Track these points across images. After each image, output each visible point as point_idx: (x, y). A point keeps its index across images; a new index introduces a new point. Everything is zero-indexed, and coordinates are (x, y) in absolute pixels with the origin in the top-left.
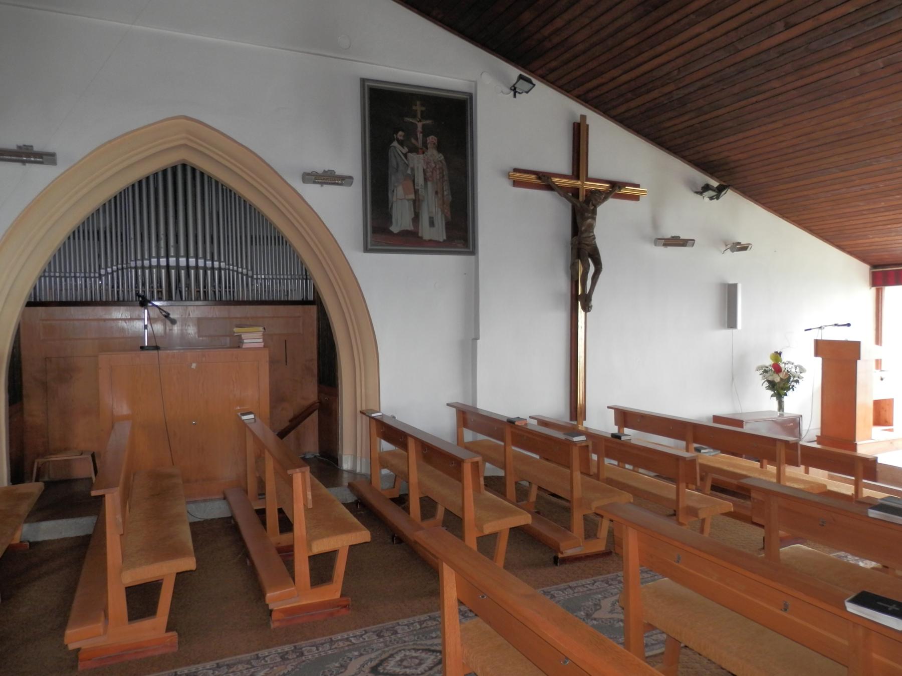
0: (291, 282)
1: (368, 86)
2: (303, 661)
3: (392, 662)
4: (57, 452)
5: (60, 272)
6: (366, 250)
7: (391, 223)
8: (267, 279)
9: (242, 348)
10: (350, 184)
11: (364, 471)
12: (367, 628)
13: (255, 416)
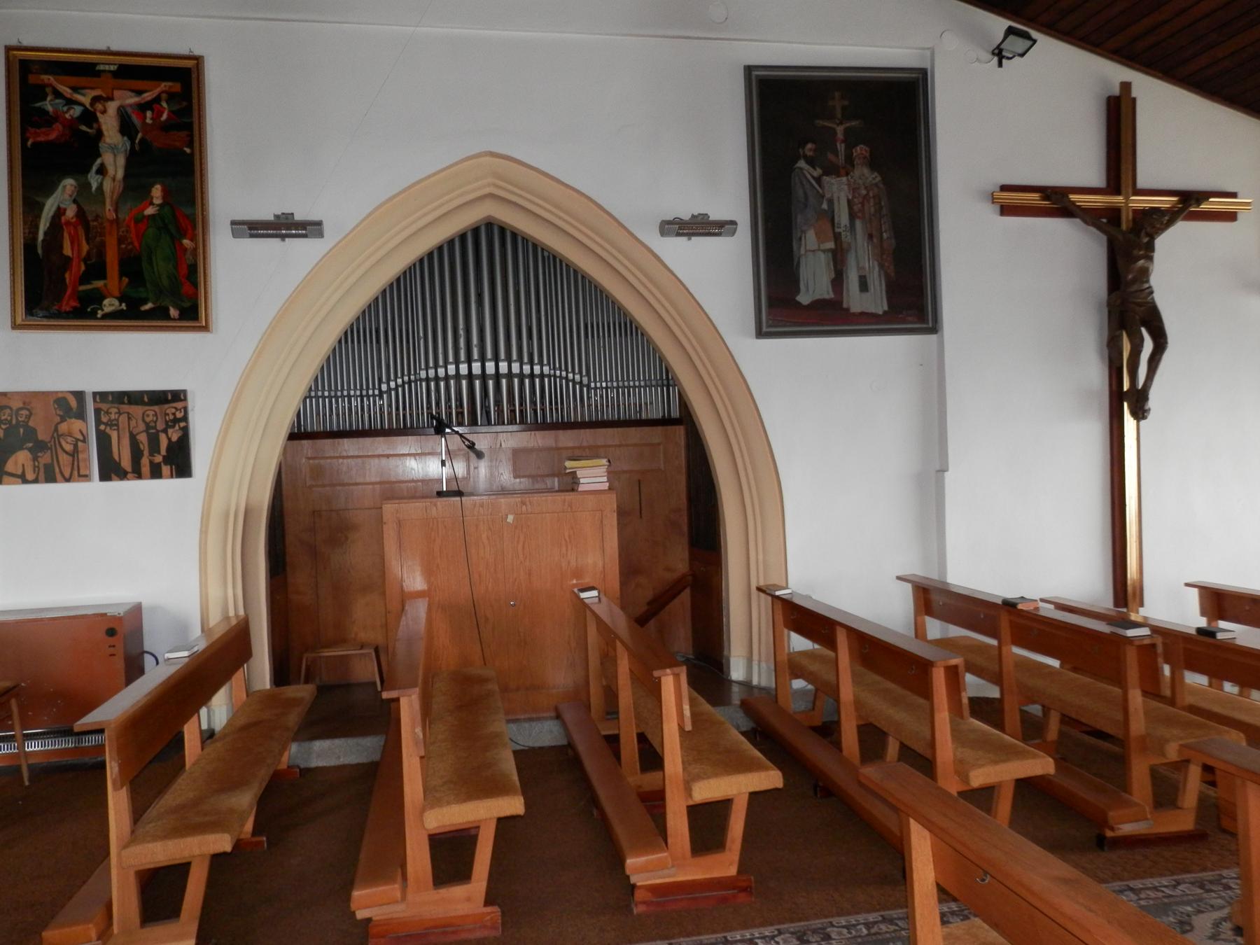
0: (645, 391)
1: (757, 76)
5: (330, 390)
6: (760, 334)
7: (798, 291)
8: (610, 388)
9: (577, 491)
10: (733, 233)
11: (764, 683)
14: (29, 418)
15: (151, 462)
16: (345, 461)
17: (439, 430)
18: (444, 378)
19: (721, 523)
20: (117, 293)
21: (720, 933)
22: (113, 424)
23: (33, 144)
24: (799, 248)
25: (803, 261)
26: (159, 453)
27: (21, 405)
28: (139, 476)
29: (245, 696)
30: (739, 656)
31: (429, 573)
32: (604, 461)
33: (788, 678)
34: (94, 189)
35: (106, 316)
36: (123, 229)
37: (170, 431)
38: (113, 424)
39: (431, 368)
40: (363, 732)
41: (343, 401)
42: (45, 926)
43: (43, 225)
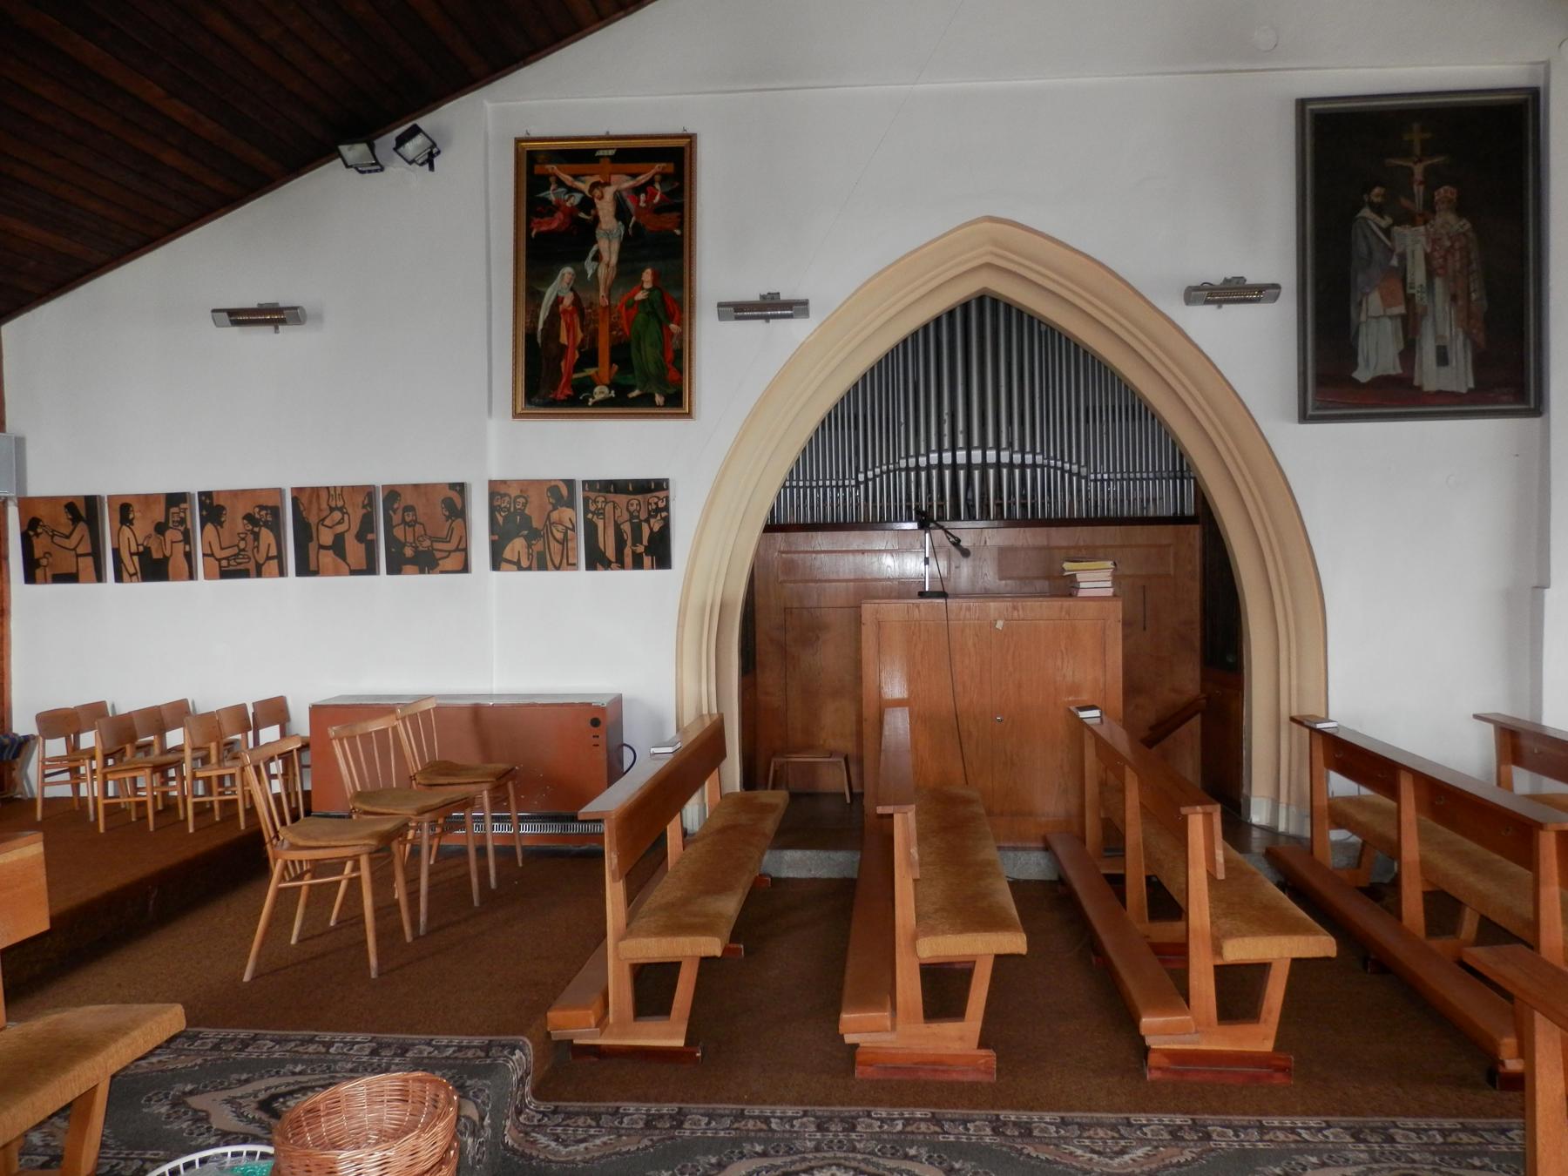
0: (1154, 484)
1: (1312, 110)
2: (1213, 1150)
4: (799, 750)
5: (805, 480)
6: (1304, 417)
7: (1355, 365)
8: (1113, 480)
9: (1076, 596)
10: (1275, 298)
11: (1293, 831)
12: (808, 1108)
13: (1101, 713)
14: (525, 506)
15: (633, 552)
16: (819, 556)
17: (925, 523)
18: (1019, 465)
19: (1245, 639)
20: (608, 382)
21: (1253, 1116)
22: (600, 513)
23: (537, 234)
24: (1359, 315)
25: (1363, 330)
26: (641, 543)
27: (518, 493)
28: (622, 566)
29: (719, 797)
30: (1263, 796)
31: (911, 681)
32: (1109, 564)
33: (1327, 828)
34: (589, 276)
35: (597, 404)
36: (616, 315)
37: (652, 521)
38: (600, 513)
39: (912, 456)
40: (836, 847)
41: (818, 492)
42: (549, 1007)
43: (543, 314)
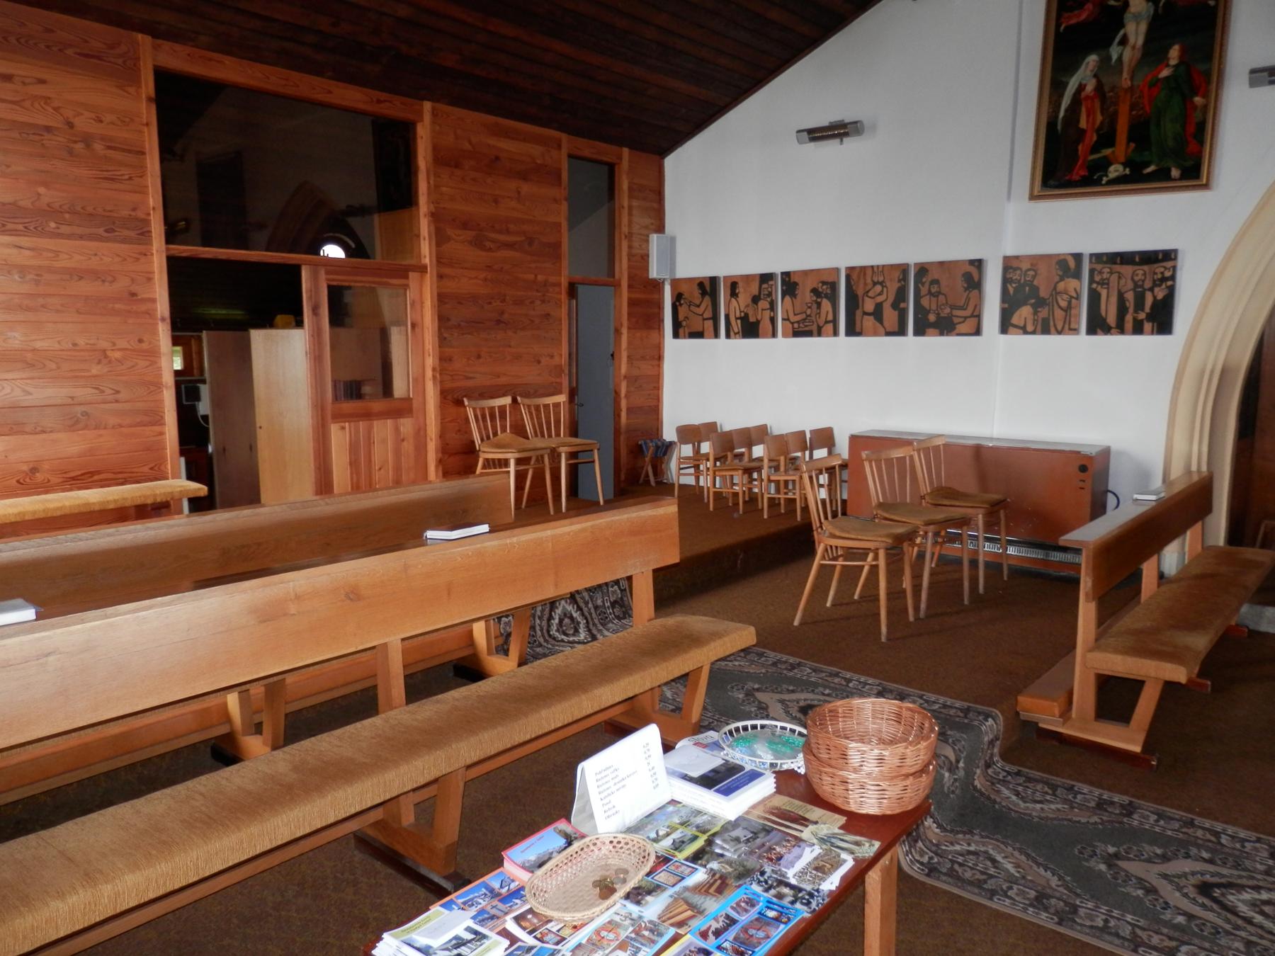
3: (1246, 896)
